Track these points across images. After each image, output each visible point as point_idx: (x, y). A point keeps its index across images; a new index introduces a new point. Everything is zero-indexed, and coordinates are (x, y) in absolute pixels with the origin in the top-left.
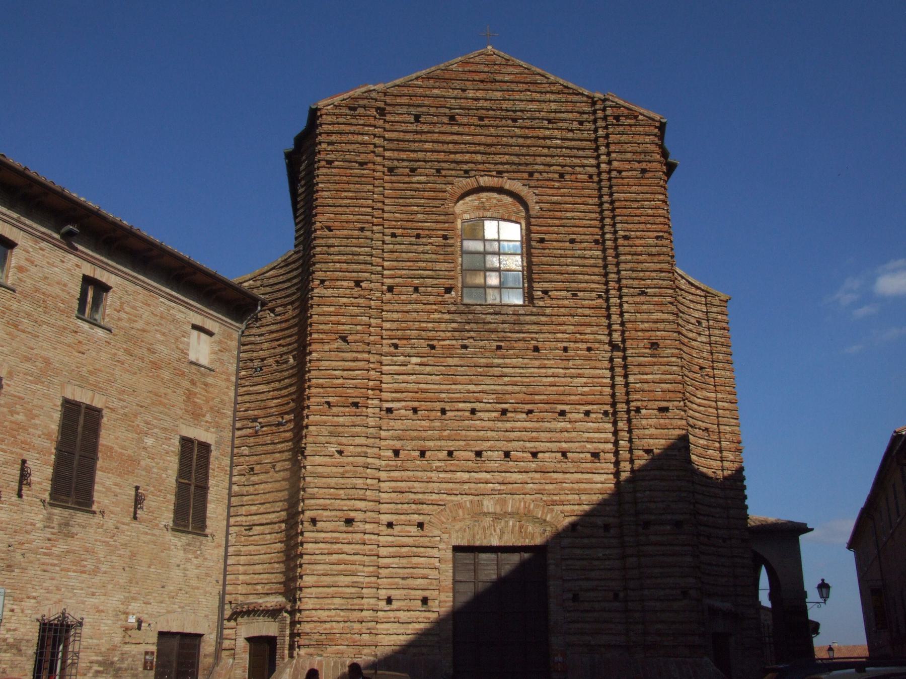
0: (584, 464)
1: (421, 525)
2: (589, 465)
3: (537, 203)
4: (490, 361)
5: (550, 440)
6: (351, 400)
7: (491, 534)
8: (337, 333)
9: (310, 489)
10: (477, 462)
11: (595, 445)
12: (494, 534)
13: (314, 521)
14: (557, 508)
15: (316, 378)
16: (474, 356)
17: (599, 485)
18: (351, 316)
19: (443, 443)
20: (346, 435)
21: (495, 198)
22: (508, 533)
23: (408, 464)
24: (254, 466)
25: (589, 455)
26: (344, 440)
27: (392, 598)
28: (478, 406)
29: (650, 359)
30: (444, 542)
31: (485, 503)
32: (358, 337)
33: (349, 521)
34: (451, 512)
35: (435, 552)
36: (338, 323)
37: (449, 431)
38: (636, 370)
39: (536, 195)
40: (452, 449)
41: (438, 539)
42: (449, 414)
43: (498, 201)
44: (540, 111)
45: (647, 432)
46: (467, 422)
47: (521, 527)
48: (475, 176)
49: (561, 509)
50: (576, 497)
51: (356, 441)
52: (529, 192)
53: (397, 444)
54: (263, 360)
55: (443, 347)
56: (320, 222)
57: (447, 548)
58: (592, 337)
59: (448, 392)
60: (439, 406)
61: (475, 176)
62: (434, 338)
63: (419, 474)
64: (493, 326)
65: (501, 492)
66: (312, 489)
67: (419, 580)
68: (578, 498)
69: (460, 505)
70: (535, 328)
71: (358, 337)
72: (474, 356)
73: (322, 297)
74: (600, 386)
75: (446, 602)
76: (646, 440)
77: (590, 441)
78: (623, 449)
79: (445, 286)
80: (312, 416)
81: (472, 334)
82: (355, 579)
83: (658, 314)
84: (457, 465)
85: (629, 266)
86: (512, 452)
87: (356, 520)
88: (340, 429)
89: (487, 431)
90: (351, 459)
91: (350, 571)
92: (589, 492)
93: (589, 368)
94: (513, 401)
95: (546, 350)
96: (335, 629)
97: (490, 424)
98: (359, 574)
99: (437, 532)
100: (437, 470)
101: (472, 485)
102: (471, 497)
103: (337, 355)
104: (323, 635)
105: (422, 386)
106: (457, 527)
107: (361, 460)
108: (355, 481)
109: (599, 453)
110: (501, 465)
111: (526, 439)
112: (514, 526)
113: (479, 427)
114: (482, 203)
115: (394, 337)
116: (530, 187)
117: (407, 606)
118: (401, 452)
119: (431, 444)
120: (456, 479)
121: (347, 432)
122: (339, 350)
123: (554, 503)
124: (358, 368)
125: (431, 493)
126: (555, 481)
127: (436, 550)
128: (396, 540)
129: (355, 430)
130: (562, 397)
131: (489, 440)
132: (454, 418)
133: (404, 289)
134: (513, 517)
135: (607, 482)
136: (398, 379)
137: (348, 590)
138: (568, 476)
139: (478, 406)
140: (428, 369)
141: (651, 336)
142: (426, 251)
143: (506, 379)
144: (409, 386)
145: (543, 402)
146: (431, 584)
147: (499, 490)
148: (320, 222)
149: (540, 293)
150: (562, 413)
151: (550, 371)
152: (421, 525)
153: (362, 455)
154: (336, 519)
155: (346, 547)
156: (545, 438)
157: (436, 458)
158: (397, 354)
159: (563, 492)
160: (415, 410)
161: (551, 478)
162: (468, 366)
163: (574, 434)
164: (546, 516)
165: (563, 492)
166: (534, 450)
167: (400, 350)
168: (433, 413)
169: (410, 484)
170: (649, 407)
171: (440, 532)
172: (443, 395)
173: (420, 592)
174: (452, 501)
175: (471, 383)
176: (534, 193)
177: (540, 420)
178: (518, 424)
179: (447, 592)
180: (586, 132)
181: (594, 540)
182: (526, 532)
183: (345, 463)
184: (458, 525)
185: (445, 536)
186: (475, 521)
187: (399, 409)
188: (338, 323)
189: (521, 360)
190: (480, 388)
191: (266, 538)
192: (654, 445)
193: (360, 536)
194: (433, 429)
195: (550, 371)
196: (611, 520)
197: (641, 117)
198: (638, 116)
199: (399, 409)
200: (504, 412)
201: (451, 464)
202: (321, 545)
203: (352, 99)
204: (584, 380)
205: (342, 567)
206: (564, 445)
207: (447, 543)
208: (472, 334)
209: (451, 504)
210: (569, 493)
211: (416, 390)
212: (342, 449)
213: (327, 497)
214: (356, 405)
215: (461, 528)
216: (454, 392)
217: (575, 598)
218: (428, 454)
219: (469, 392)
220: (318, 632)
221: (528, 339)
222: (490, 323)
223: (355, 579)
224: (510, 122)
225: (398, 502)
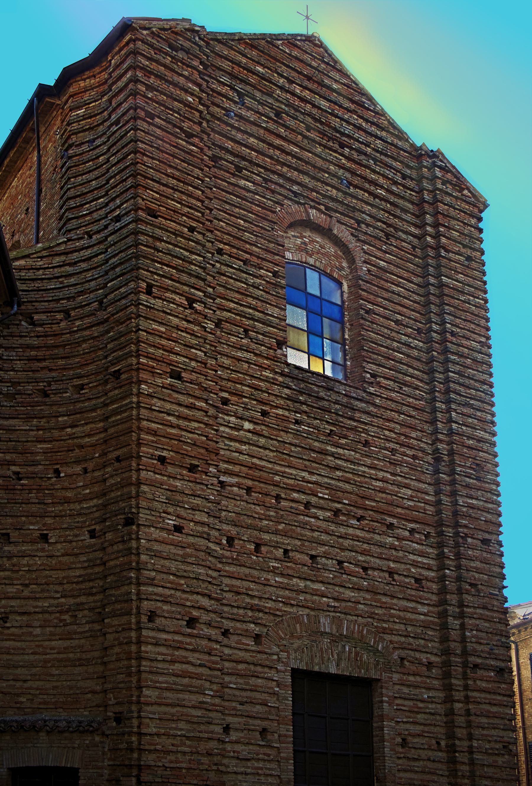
0: (409, 590)
1: (257, 638)
2: (413, 593)
3: (365, 262)
4: (323, 446)
5: (380, 556)
6: (188, 461)
7: (329, 659)
8: (170, 364)
9: (145, 572)
10: (313, 569)
11: (419, 570)
12: (332, 659)
13: (152, 616)
14: (387, 637)
15: (148, 420)
16: (310, 436)
17: (422, 617)
18: (185, 345)
19: (278, 539)
20: (186, 506)
21: (317, 242)
22: (345, 660)
23: (243, 559)
24: (9, 531)
25: (413, 581)
26: (183, 513)
27: (231, 726)
28: (313, 500)
29: (475, 481)
30: (282, 662)
31: (321, 621)
32: (194, 376)
33: (192, 622)
34: (289, 626)
35: (272, 674)
36: (171, 351)
37: (284, 525)
38: (464, 492)
39: (365, 252)
40: (289, 548)
41: (275, 657)
42: (283, 503)
43: (322, 247)
44: (367, 145)
45: (472, 564)
46: (302, 517)
47: (357, 654)
48: (304, 204)
49: (390, 639)
50: (402, 627)
51: (196, 517)
52: (356, 247)
53: (233, 531)
54: (14, 384)
55: (277, 416)
56: (143, 199)
57: (286, 670)
58: (415, 442)
59: (283, 475)
60: (274, 491)
61: (304, 204)
62: (268, 402)
63: (255, 573)
64: (325, 404)
65: (336, 610)
66: (148, 572)
67: (258, 707)
68: (404, 629)
69: (297, 619)
70: (365, 418)
71: (194, 376)
72: (310, 436)
73: (150, 308)
74: (424, 503)
75: (286, 736)
76: (471, 573)
77: (415, 564)
78: (450, 579)
79: (278, 338)
80: (144, 472)
81: (304, 408)
82: (201, 698)
83: (482, 433)
84: (293, 569)
85: (457, 368)
86: (345, 564)
87: (200, 621)
88: (178, 497)
89: (322, 532)
90: (191, 540)
91: (196, 687)
92: (415, 623)
93: (415, 480)
94: (347, 502)
95: (376, 447)
96: (182, 762)
97: (324, 525)
98: (207, 692)
99: (275, 649)
100: (274, 571)
101: (308, 597)
102: (307, 611)
103: (170, 394)
104: (168, 769)
105: (255, 460)
106: (295, 646)
107: (202, 542)
108: (196, 569)
109: (421, 580)
110: (335, 576)
111: (359, 550)
112: (350, 652)
113: (314, 525)
114: (305, 243)
115: (226, 389)
116: (359, 240)
117: (246, 738)
118: (236, 541)
119: (266, 537)
120: (293, 585)
121: (187, 503)
122: (172, 388)
123: (384, 631)
124: (195, 419)
125: (268, 598)
126: (385, 606)
127: (273, 672)
128: (233, 654)
129: (195, 501)
130: (391, 508)
131: (323, 545)
132: (289, 510)
133: (234, 328)
134: (349, 642)
135: (430, 614)
136: (231, 446)
137: (194, 712)
138: (395, 601)
139: (313, 500)
140: (262, 441)
141: (476, 456)
142: (256, 285)
143: (338, 473)
144: (242, 457)
145: (374, 509)
146: (270, 713)
147: (335, 607)
148: (143, 199)
149: (368, 376)
150: (391, 526)
151: (381, 474)
152: (257, 638)
153: (205, 536)
154: (179, 617)
155: (193, 657)
156: (377, 552)
157: (273, 557)
158: (229, 413)
159: (392, 620)
160: (249, 490)
161: (379, 601)
162: (302, 447)
163: (401, 554)
164: (378, 646)
165: (392, 620)
166: (366, 565)
167: (231, 407)
168: (267, 499)
169: (246, 584)
170: (475, 536)
171: (278, 650)
172: (277, 478)
173: (258, 722)
174: (290, 613)
175: (305, 469)
176: (363, 249)
177: (371, 530)
178: (351, 531)
179: (287, 724)
180: (409, 192)
181: (419, 679)
182: (361, 661)
183: (185, 543)
184: (297, 643)
185: (284, 655)
186: (313, 641)
187: (232, 486)
188: (171, 351)
189: (353, 453)
190: (314, 478)
191: (34, 633)
192: (479, 580)
193: (204, 642)
194: (268, 518)
195: (381, 474)
196: (433, 659)
197: (466, 192)
198: (464, 189)
199: (232, 486)
200: (337, 512)
201: (288, 567)
202: (163, 650)
203: (173, 32)
204: (409, 492)
205: (186, 681)
206: (392, 565)
207: (286, 664)
208: (304, 408)
209: (289, 616)
210: (398, 621)
211: (250, 465)
212: (181, 525)
213: (168, 585)
214: (192, 469)
215: (299, 647)
216: (288, 476)
217: (404, 743)
218: (263, 549)
219: (304, 480)
220: (164, 766)
221: (360, 429)
222: (323, 399)
223: (201, 698)
224: (336, 146)
225: (234, 604)
